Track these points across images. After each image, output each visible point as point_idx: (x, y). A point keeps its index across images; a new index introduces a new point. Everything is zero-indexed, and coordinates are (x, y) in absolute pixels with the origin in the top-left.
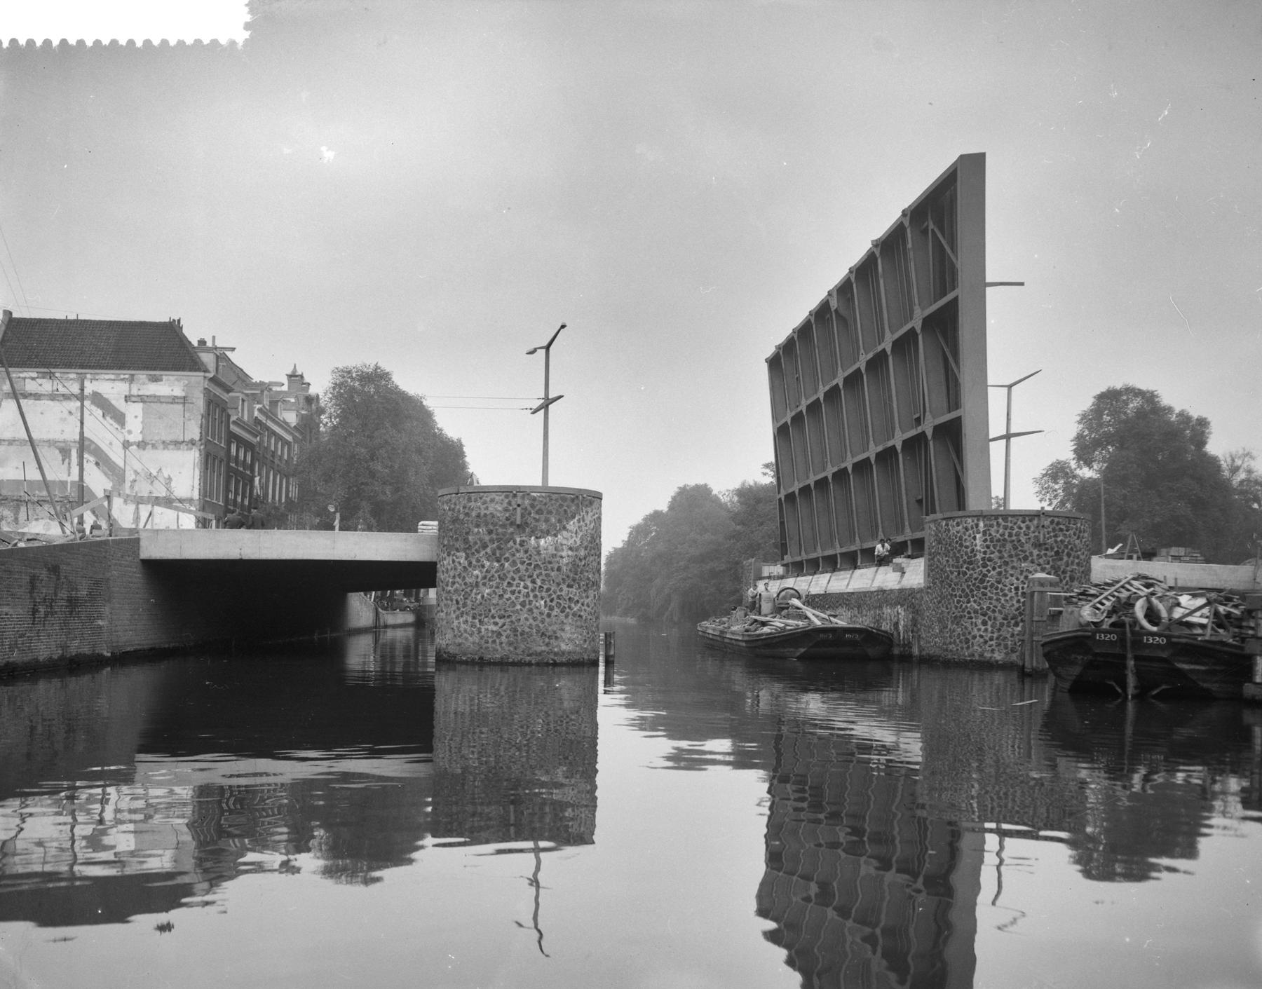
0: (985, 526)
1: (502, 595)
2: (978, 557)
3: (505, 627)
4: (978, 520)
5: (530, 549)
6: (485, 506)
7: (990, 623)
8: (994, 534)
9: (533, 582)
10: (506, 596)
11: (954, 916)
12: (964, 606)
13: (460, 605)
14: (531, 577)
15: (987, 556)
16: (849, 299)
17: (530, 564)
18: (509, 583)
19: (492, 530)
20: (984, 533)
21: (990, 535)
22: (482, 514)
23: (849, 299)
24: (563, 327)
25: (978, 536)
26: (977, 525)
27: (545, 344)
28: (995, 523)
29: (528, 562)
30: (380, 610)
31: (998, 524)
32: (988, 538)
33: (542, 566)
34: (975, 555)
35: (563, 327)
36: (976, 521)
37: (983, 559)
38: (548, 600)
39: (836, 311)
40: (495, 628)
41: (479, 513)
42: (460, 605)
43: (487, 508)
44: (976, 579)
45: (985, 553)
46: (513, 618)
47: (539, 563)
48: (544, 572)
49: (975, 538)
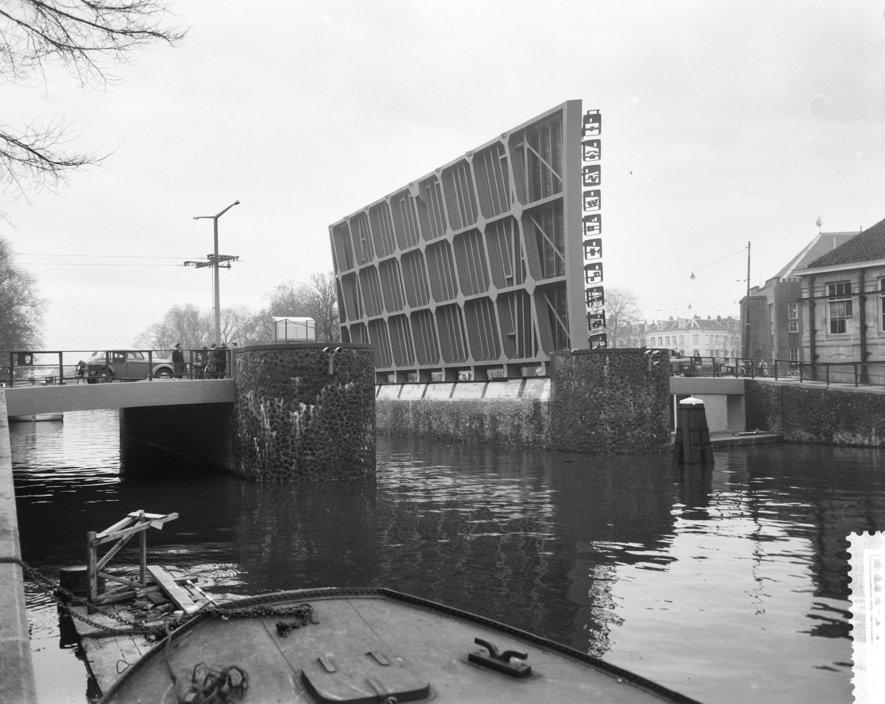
0: (610, 360)
1: (318, 431)
2: (606, 382)
3: (321, 457)
4: (605, 356)
5: (339, 393)
6: (300, 360)
7: (617, 428)
8: (617, 366)
9: (342, 420)
10: (321, 432)
11: (175, 602)
12: (596, 417)
13: (280, 441)
14: (340, 415)
15: (613, 381)
16: (428, 190)
17: (338, 405)
18: (323, 421)
19: (307, 380)
20: (610, 364)
21: (614, 366)
22: (298, 366)
23: (428, 190)
24: (237, 203)
25: (605, 367)
26: (605, 360)
27: (214, 215)
28: (617, 358)
29: (337, 404)
30: (818, 503)
31: (620, 359)
32: (613, 368)
33: (347, 406)
34: (604, 380)
35: (237, 203)
36: (603, 356)
37: (610, 383)
38: (352, 433)
39: (417, 198)
40: (313, 458)
41: (296, 366)
42: (280, 441)
43: (302, 362)
44: (605, 397)
45: (611, 379)
46: (327, 450)
47: (345, 404)
48: (348, 411)
49: (603, 369)
